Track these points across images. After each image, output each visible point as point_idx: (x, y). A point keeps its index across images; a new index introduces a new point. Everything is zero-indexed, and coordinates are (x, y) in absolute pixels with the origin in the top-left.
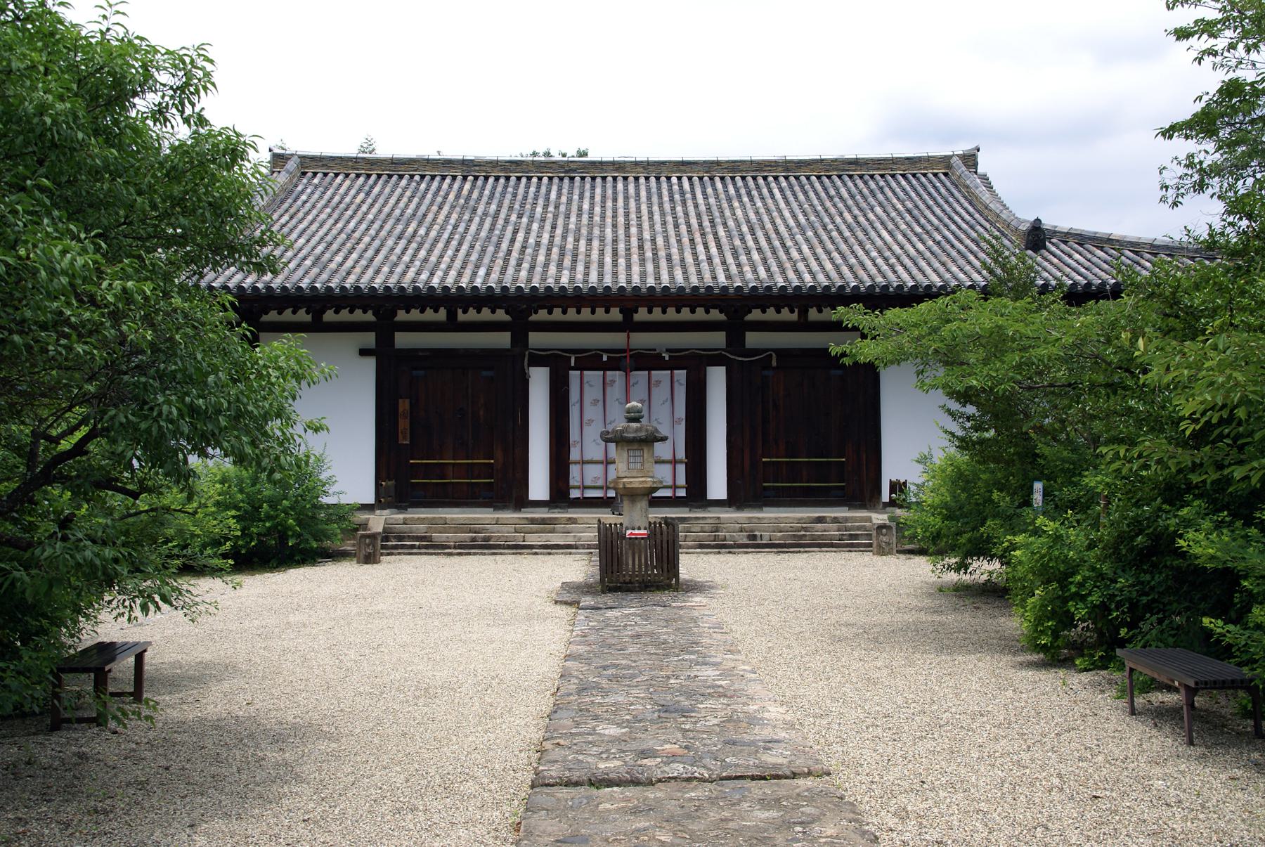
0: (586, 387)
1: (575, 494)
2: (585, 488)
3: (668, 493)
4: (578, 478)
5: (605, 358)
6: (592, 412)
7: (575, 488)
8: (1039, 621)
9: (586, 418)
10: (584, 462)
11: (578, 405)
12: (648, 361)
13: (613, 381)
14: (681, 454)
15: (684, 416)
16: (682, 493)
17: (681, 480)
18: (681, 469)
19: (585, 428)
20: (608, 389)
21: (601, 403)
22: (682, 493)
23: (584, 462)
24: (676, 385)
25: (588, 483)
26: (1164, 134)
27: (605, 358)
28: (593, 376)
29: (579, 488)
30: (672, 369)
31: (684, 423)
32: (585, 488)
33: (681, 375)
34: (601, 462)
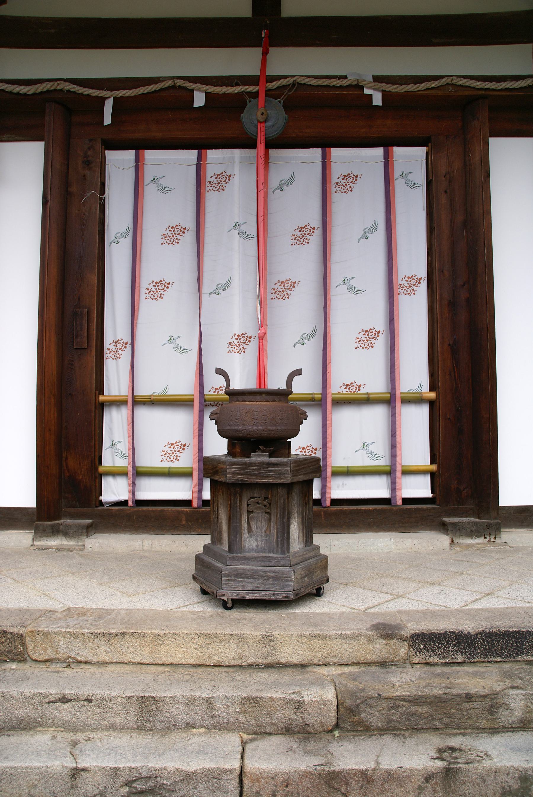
0: (150, 193)
1: (114, 490)
2: (139, 473)
3: (376, 489)
4: (124, 447)
5: (199, 100)
6: (165, 261)
7: (115, 473)
8: (325, 466)
9: (146, 280)
10: (138, 402)
11: (127, 243)
12: (325, 119)
13: (225, 178)
14: (415, 374)
15: (422, 272)
16: (419, 488)
17: (416, 448)
18: (416, 424)
19: (146, 306)
20: (212, 199)
21: (189, 238)
22: (419, 488)
23: (138, 402)
24: (399, 186)
25: (149, 459)
26: (363, 241)
27: (199, 100)
28: (172, 166)
29: (123, 473)
30: (387, 143)
31: (423, 290)
32: (139, 473)
33: (411, 159)
34: (341, 402)
